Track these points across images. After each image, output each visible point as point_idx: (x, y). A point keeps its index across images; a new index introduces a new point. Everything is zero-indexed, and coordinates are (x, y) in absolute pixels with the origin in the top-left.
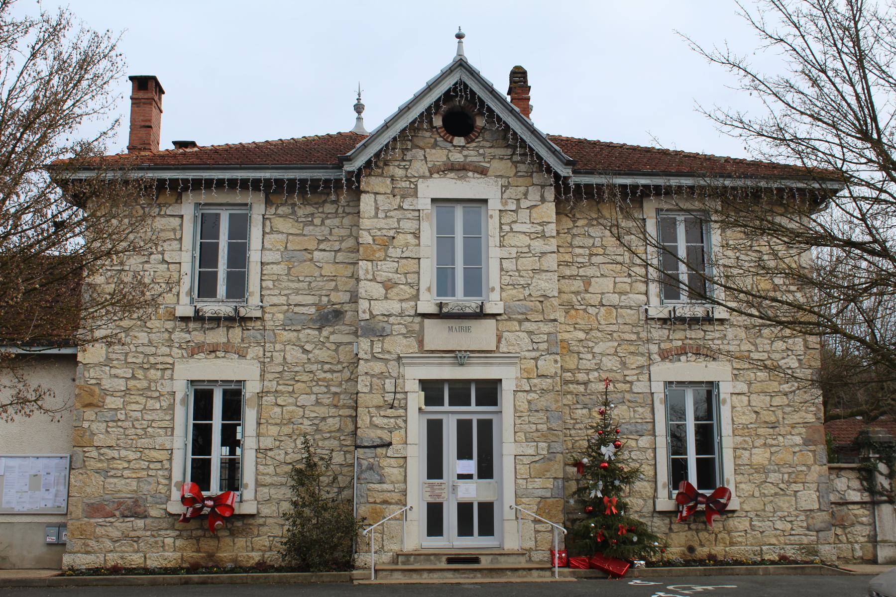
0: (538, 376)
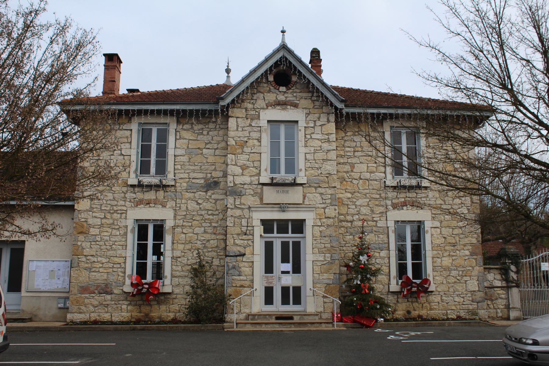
0: (326, 218)
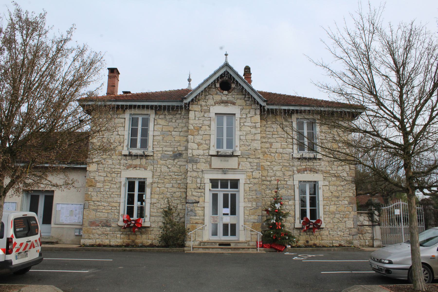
0: (253, 178)
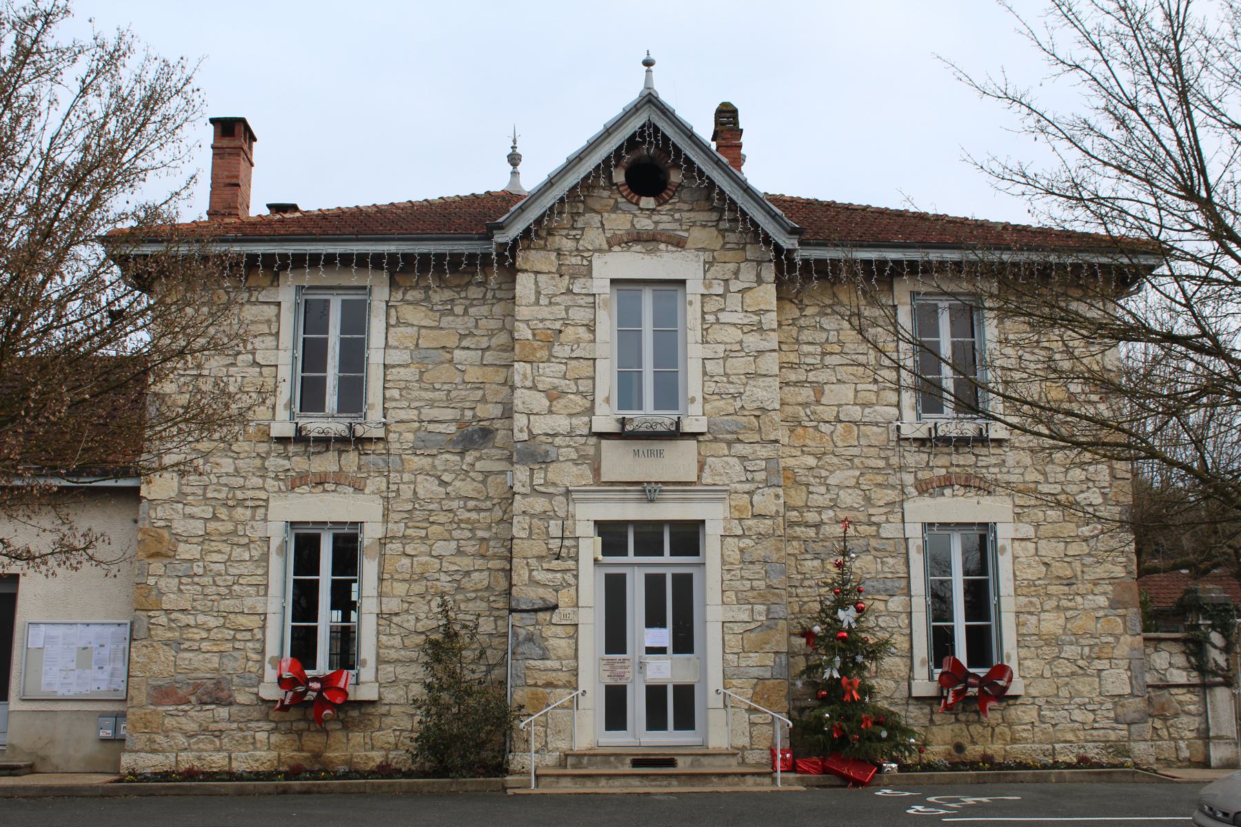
0: (754, 516)
